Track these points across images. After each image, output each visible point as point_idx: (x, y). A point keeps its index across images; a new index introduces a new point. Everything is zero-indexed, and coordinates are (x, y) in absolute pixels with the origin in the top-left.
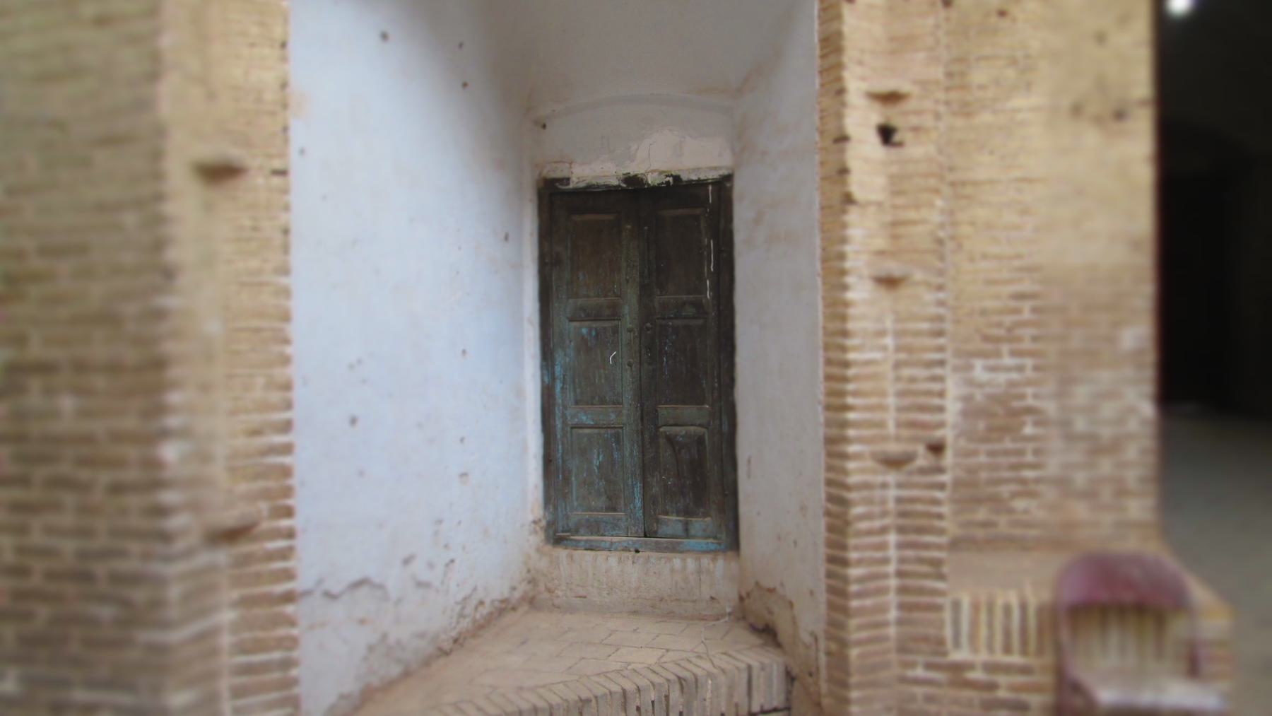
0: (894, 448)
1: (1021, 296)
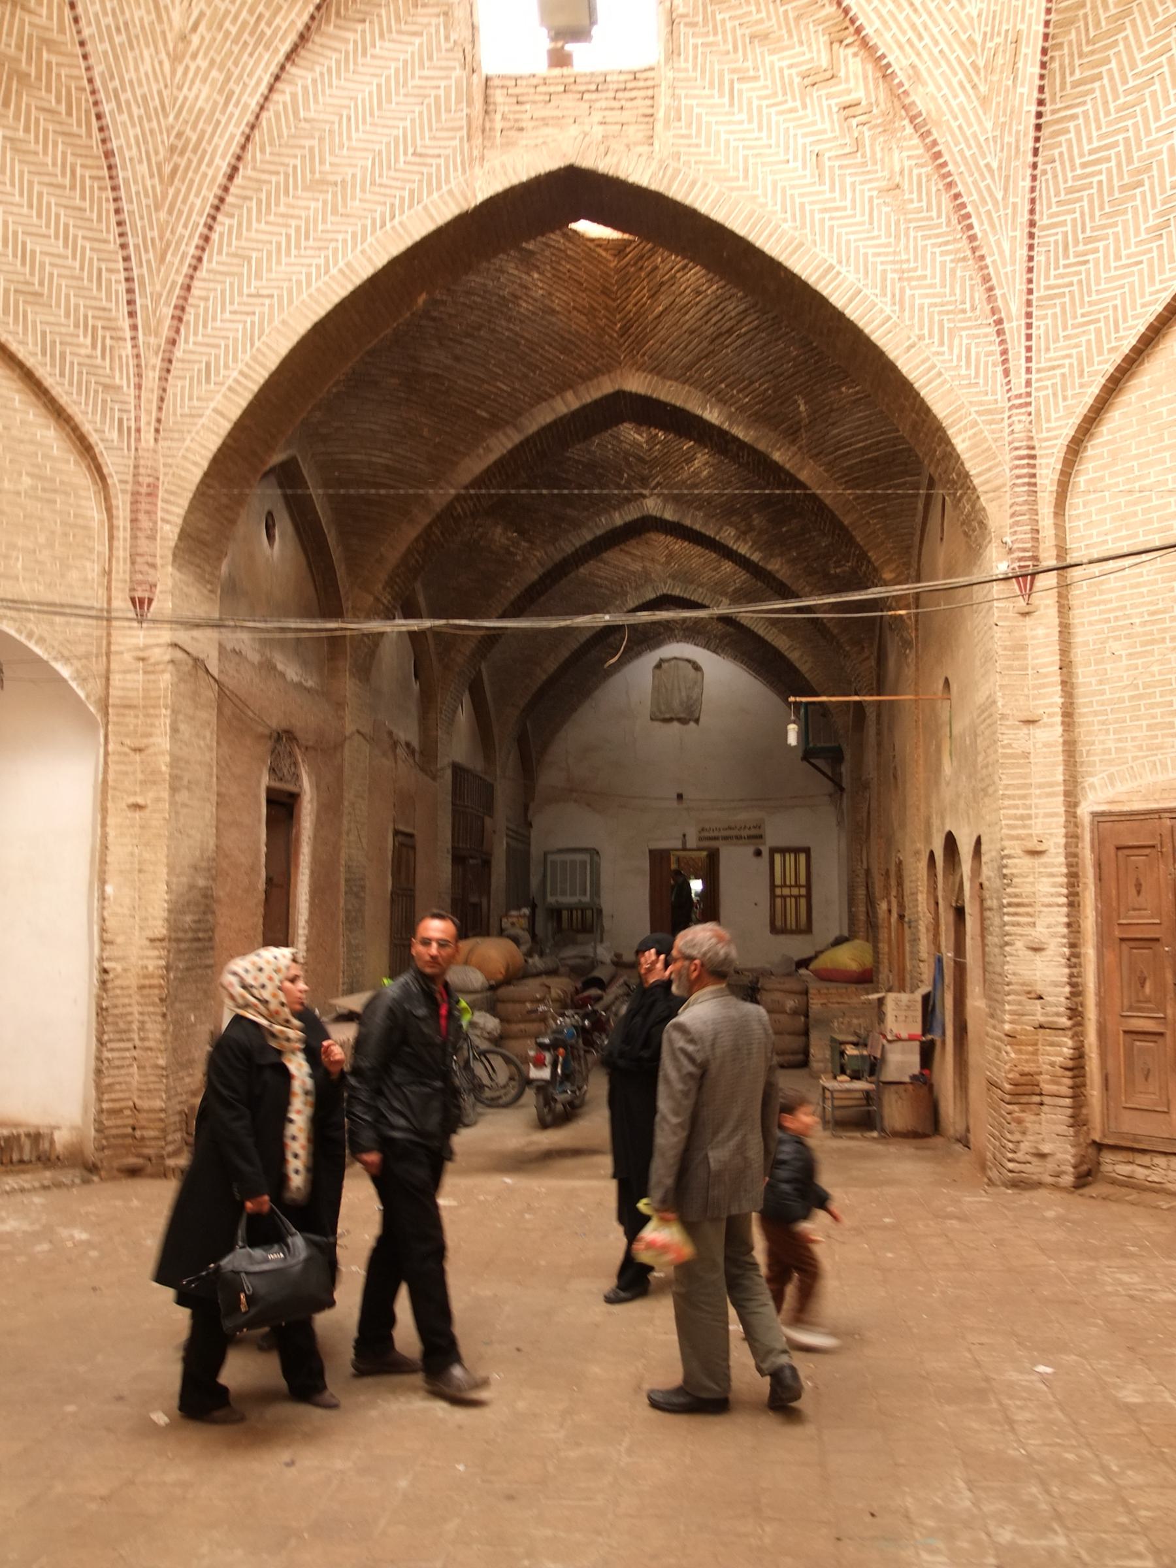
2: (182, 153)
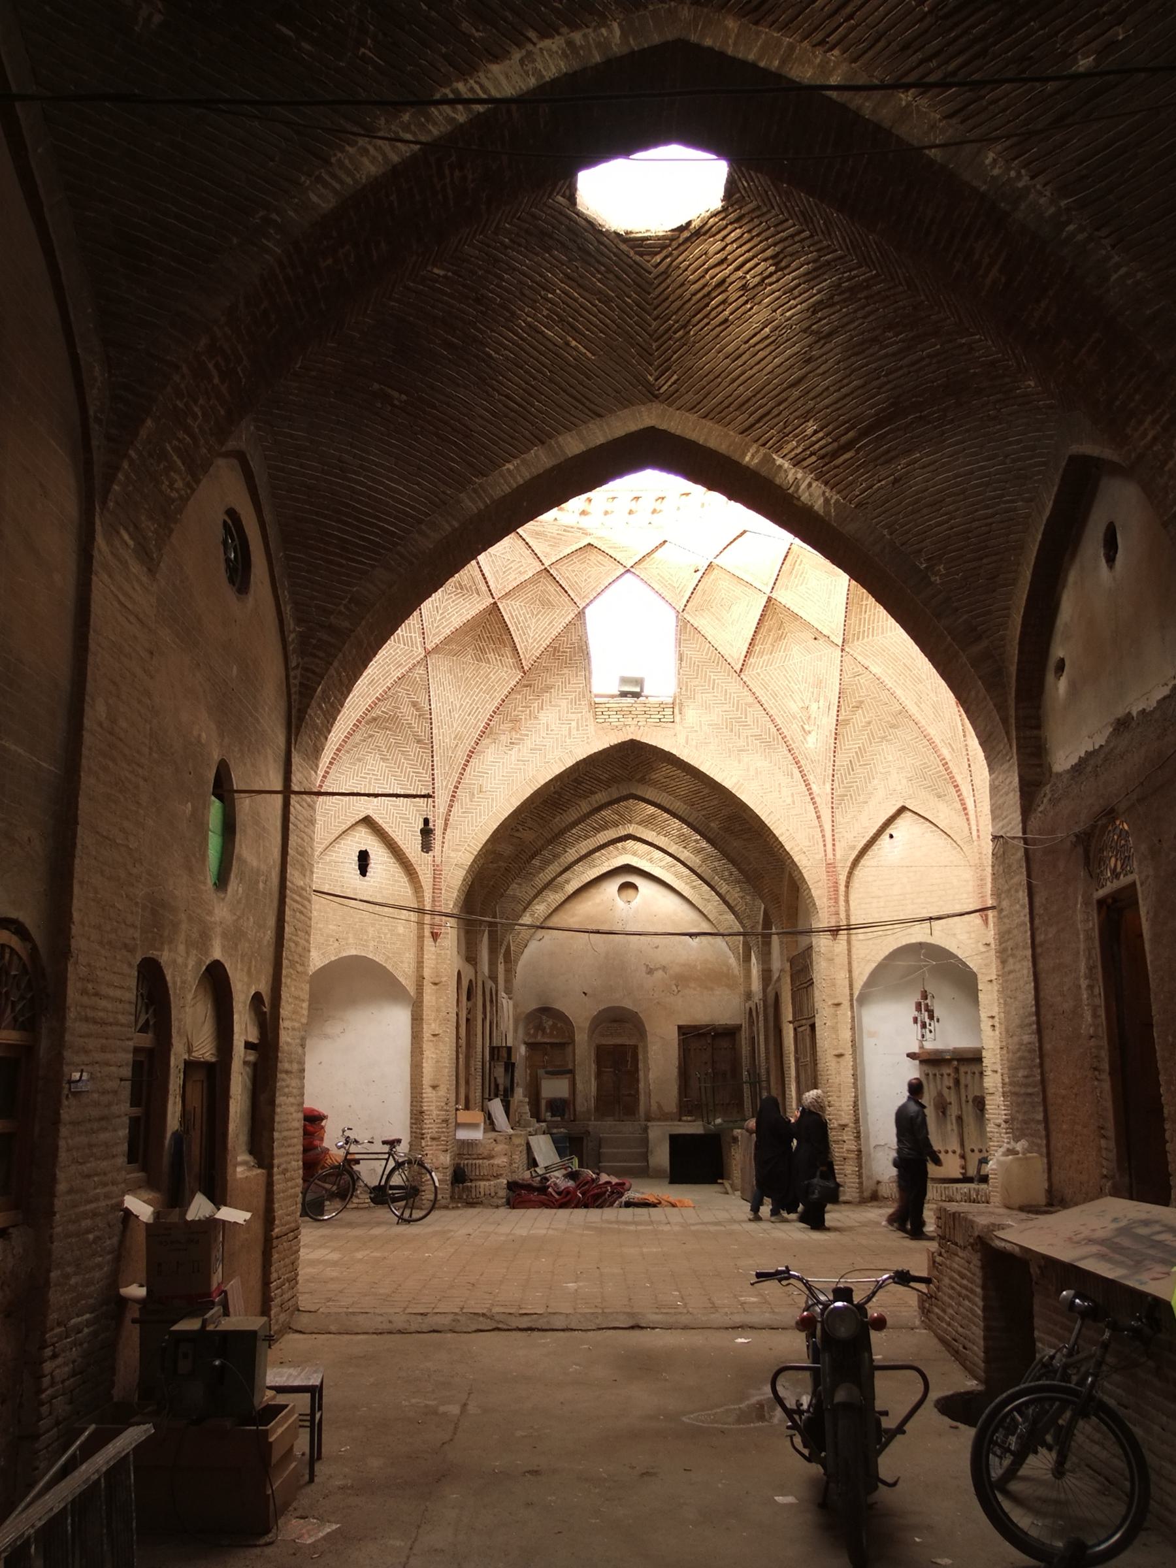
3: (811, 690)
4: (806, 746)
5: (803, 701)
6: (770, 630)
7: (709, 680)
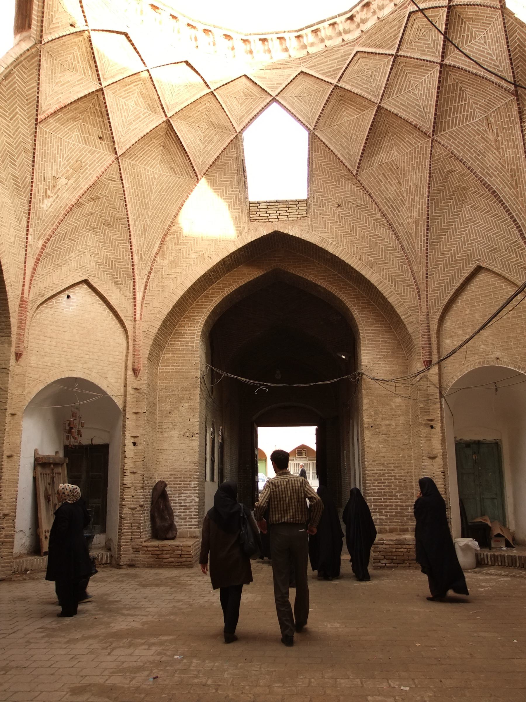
0: (133, 506)
1: (172, 475)
2: (515, 175)
3: (68, 168)
4: (42, 206)
5: (57, 172)
6: (75, 109)
7: (13, 111)
